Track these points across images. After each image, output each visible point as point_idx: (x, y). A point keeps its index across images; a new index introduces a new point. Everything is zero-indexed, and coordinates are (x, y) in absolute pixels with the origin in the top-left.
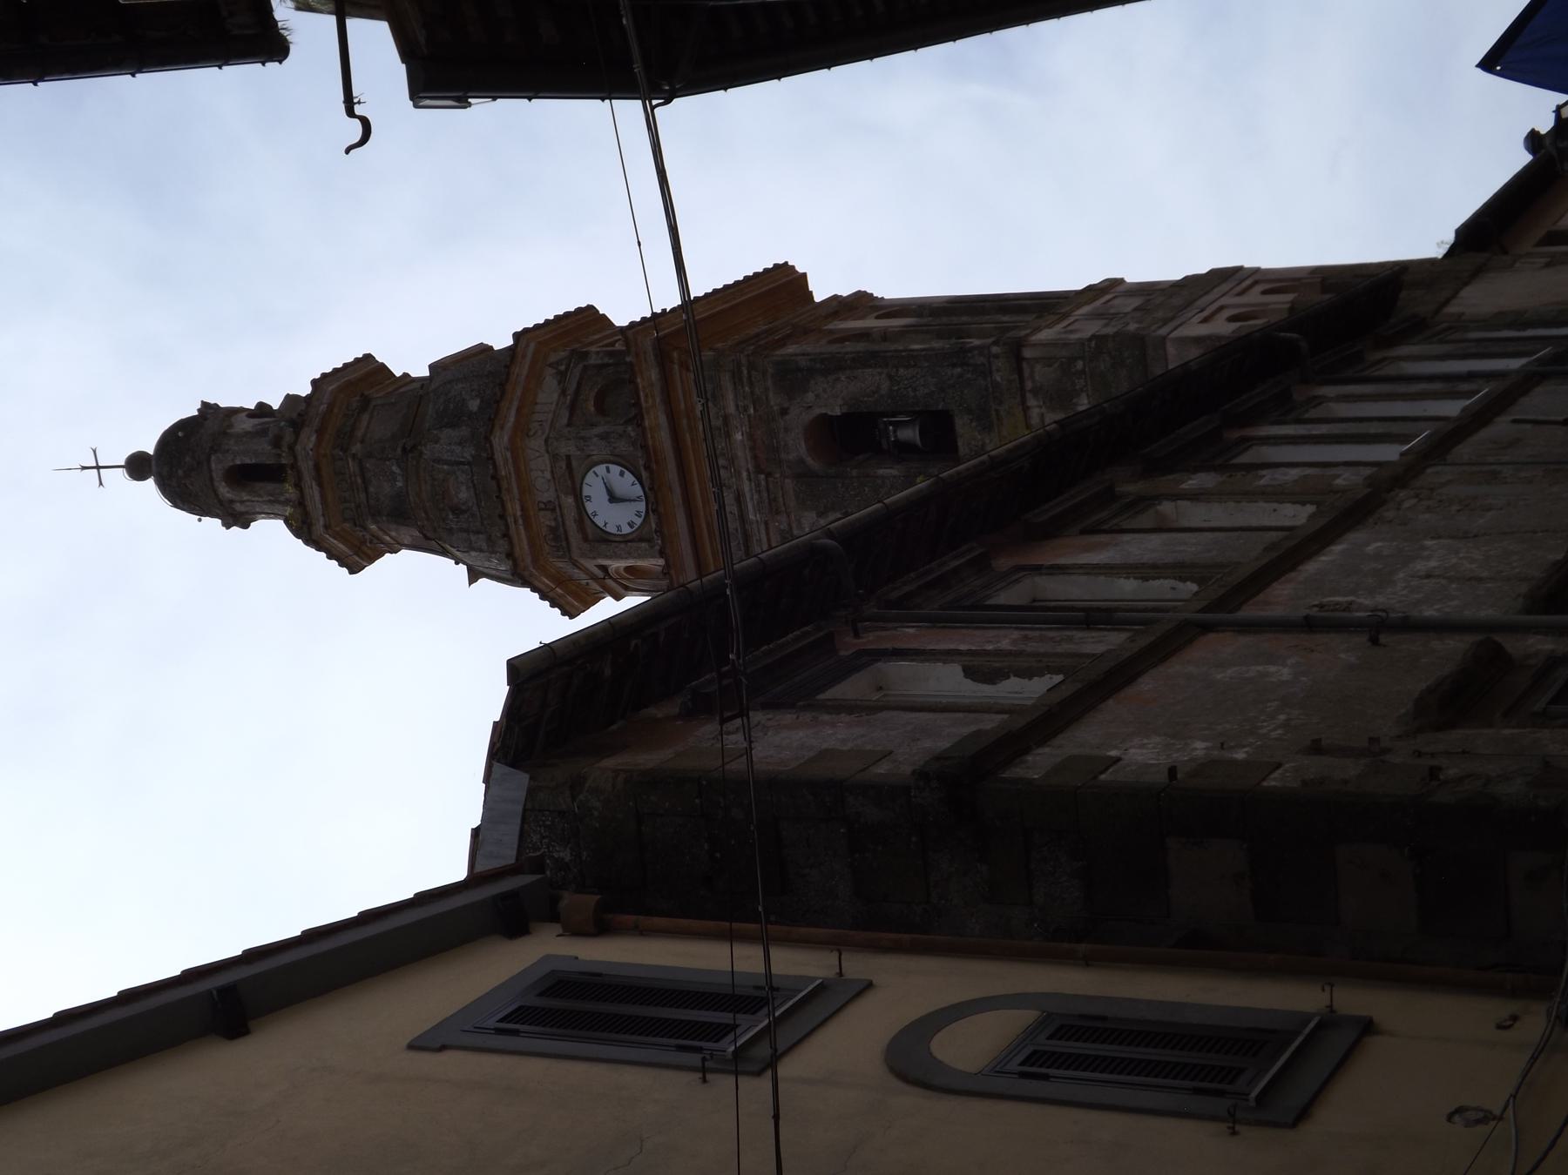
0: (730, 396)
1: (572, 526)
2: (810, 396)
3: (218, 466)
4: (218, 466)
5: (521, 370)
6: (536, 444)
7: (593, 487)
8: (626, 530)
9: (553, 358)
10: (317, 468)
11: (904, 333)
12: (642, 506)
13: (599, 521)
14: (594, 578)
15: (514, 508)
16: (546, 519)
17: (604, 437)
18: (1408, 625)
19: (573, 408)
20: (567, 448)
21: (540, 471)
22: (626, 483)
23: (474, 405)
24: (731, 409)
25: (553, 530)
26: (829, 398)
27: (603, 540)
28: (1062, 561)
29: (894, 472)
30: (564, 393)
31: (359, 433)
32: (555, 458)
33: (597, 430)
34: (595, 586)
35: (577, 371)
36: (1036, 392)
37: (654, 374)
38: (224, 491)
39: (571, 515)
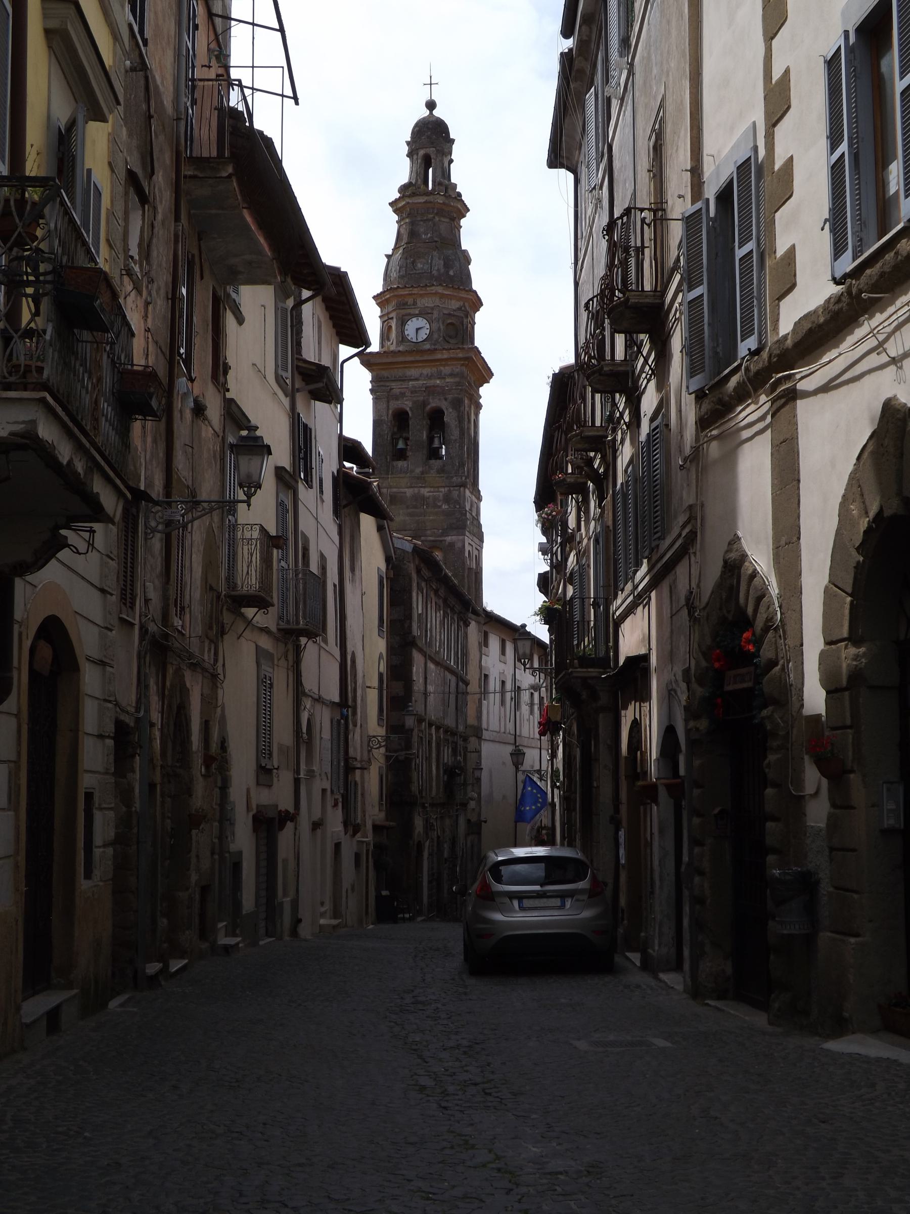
0: (452, 380)
1: (408, 311)
2: (451, 410)
3: (431, 151)
4: (431, 151)
5: (463, 295)
6: (437, 301)
7: (421, 322)
8: (406, 333)
9: (466, 304)
10: (431, 202)
11: (469, 435)
12: (414, 340)
13: (409, 322)
14: (388, 313)
15: (415, 291)
16: (410, 301)
17: (439, 329)
18: (426, 698)
19: (449, 314)
20: (435, 315)
21: (426, 302)
22: (423, 335)
23: (451, 273)
24: (448, 380)
25: (406, 304)
26: (449, 417)
27: (402, 323)
28: (323, 328)
29: (425, 437)
30: (454, 310)
31: (443, 219)
32: (432, 309)
33: (442, 327)
34: (386, 311)
35: (462, 315)
36: (450, 491)
37: (460, 355)
38: (422, 152)
39: (411, 311)
